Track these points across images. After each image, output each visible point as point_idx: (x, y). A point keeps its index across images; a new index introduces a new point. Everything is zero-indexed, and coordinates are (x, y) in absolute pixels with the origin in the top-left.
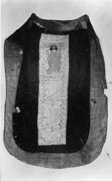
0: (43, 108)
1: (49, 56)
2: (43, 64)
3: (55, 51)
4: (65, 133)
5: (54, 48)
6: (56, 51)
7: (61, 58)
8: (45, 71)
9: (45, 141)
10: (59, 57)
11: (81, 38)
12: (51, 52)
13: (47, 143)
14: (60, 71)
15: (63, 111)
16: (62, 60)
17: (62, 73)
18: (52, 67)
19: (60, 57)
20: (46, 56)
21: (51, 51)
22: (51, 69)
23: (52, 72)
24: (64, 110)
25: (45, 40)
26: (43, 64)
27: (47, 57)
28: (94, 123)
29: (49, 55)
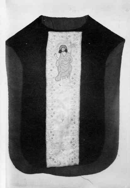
0: (52, 124)
1: (57, 60)
2: (53, 67)
3: (64, 53)
4: (78, 132)
5: (63, 49)
6: (66, 54)
7: (72, 61)
8: (54, 78)
9: (55, 162)
10: (70, 61)
11: (100, 45)
12: (61, 54)
13: (57, 164)
14: (71, 78)
15: (74, 126)
16: (73, 64)
17: (73, 161)
18: (61, 73)
19: (70, 61)
20: (54, 61)
21: (60, 54)
22: (60, 75)
23: (62, 79)
24: (75, 124)
25: (55, 39)
26: (51, 70)
27: (56, 60)
28: (111, 56)
29: (58, 59)
